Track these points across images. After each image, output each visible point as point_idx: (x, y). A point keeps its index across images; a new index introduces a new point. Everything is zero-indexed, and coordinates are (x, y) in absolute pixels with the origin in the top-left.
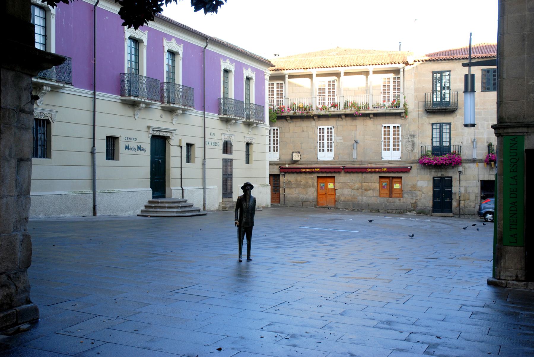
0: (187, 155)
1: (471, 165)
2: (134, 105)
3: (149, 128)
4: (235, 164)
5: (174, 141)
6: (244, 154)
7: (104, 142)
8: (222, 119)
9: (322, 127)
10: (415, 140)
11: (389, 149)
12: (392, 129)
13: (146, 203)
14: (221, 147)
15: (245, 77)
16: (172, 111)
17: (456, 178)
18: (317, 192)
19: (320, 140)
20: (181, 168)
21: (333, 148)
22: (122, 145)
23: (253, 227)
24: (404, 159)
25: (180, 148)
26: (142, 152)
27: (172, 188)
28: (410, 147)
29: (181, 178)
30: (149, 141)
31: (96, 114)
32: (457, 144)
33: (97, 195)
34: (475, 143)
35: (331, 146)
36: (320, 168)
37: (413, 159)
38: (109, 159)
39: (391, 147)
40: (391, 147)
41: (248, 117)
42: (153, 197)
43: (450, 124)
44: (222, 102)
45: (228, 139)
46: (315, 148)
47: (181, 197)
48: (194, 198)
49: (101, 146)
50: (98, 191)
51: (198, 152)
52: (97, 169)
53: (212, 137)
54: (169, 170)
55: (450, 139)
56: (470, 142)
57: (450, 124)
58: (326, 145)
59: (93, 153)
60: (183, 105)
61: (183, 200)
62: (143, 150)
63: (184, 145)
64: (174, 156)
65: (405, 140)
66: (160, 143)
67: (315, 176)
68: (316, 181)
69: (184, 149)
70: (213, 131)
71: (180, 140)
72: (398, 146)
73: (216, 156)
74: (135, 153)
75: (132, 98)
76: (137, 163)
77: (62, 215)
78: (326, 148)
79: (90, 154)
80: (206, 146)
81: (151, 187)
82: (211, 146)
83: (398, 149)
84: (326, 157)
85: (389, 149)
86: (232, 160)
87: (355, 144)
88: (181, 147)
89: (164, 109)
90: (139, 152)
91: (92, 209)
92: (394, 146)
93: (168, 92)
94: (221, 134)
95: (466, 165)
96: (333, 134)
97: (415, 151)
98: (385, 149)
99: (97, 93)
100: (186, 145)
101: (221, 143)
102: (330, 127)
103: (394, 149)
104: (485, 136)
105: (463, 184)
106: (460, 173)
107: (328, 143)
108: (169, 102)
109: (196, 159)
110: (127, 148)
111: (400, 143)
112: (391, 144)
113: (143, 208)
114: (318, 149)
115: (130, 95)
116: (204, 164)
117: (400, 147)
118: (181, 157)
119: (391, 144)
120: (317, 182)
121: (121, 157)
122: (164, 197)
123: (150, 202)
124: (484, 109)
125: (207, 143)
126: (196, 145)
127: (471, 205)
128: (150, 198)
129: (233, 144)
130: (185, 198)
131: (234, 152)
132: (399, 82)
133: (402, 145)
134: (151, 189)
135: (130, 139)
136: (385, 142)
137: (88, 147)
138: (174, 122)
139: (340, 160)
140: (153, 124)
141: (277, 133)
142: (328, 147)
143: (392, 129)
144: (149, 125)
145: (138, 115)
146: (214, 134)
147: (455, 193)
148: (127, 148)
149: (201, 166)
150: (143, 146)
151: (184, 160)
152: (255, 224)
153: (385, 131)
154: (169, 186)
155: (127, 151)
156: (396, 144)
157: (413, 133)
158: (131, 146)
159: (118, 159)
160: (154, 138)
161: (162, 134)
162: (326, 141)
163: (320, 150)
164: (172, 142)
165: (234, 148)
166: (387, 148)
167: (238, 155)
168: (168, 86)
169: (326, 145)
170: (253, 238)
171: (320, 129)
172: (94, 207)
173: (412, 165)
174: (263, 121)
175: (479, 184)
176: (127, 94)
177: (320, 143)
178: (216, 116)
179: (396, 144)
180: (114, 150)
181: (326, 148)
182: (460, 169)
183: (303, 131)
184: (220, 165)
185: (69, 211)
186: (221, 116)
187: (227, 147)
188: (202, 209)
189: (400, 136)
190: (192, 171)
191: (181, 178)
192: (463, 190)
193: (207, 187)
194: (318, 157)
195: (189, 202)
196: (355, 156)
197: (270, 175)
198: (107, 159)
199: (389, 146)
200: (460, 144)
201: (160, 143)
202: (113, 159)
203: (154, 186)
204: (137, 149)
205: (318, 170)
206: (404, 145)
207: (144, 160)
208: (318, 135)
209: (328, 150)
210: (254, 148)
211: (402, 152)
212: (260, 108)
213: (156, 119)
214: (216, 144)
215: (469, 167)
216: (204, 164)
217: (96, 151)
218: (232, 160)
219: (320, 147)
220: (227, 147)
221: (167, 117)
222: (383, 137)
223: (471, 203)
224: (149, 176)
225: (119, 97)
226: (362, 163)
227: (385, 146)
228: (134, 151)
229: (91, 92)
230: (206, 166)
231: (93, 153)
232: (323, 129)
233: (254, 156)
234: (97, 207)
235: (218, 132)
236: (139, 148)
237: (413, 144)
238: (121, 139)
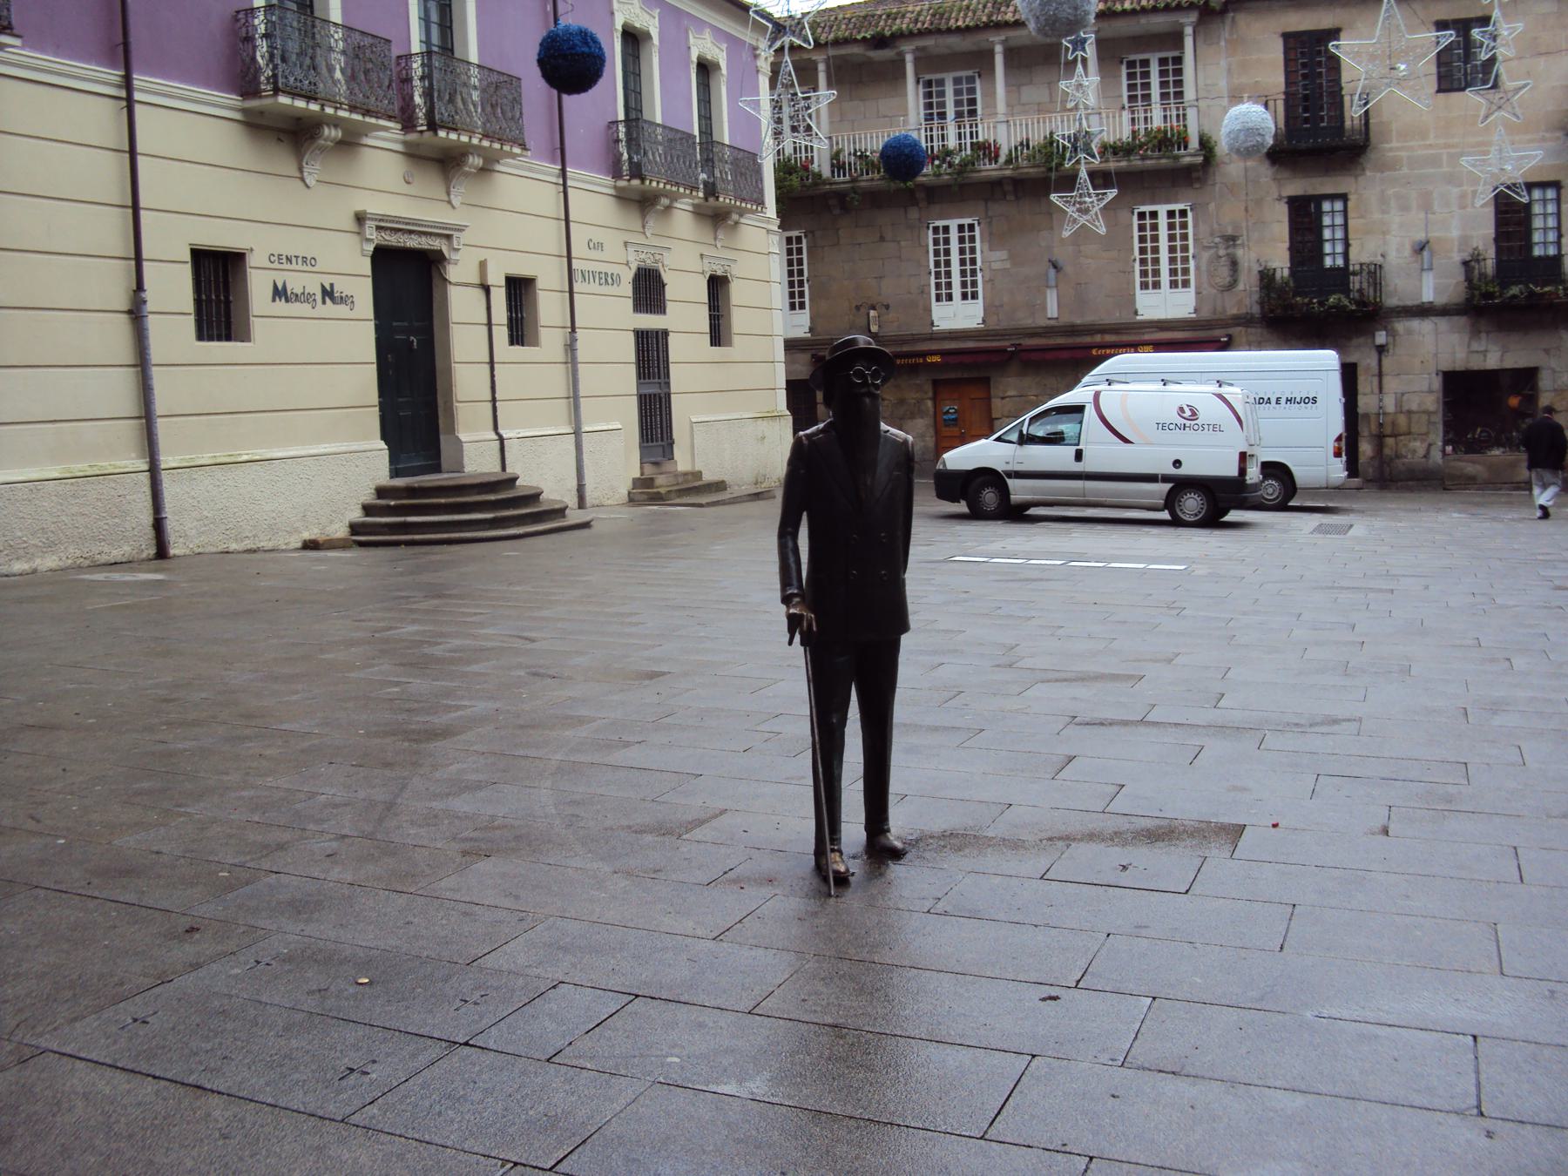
0: (510, 319)
1: (1415, 324)
2: (297, 135)
3: (360, 218)
4: (677, 348)
5: (459, 270)
6: (704, 312)
7: (186, 273)
8: (622, 197)
9: (940, 223)
10: (1240, 252)
11: (1157, 285)
12: (1163, 221)
13: (368, 496)
14: (627, 289)
15: (695, 59)
16: (447, 163)
17: (1368, 368)
18: (937, 432)
19: (937, 264)
20: (492, 363)
21: (980, 289)
22: (258, 285)
23: (905, 640)
24: (1206, 314)
25: (480, 294)
26: (342, 310)
27: (463, 437)
28: (1224, 273)
29: (494, 400)
30: (366, 266)
31: (142, 162)
32: (1365, 259)
33: (166, 480)
34: (1425, 253)
35: (974, 284)
36: (942, 353)
37: (1235, 311)
38: (211, 339)
39: (1165, 277)
40: (1165, 277)
41: (711, 191)
42: (395, 473)
43: (1344, 197)
44: (622, 136)
45: (649, 263)
46: (924, 291)
47: (498, 469)
48: (544, 472)
49: (172, 289)
50: (166, 460)
51: (548, 307)
52: (158, 376)
53: (594, 254)
54: (448, 371)
55: (1347, 245)
56: (1407, 252)
57: (1344, 197)
58: (956, 279)
59: (136, 313)
60: (486, 136)
61: (504, 477)
62: (343, 300)
63: (497, 279)
64: (467, 319)
65: (1206, 255)
66: (407, 281)
67: (924, 381)
68: (930, 394)
69: (499, 297)
70: (598, 235)
71: (483, 265)
72: (1186, 271)
73: (611, 322)
74: (314, 313)
75: (284, 100)
76: (323, 351)
77: (18, 567)
78: (957, 290)
79: (124, 318)
80: (577, 287)
81: (384, 437)
82: (594, 287)
83: (1186, 284)
84: (958, 315)
85: (1157, 285)
86: (666, 333)
87: (1052, 272)
88: (486, 289)
89: (413, 154)
90: (330, 309)
91: (150, 533)
92: (1173, 272)
93: (428, 94)
94: (626, 244)
95: (1401, 326)
96: (978, 244)
97: (1241, 287)
98: (1144, 286)
99: (139, 80)
100: (503, 283)
101: (628, 276)
102: (966, 221)
103: (1174, 284)
104: (1455, 233)
105: (1391, 384)
106: (1381, 350)
107: (963, 273)
108: (433, 126)
109: (543, 331)
110: (279, 293)
111: (1192, 264)
112: (1164, 267)
113: (356, 515)
114: (933, 292)
115: (277, 91)
116: (571, 347)
117: (1192, 277)
118: (489, 324)
119: (1164, 267)
120: (934, 399)
121: (257, 326)
122: (437, 469)
123: (381, 492)
124: (1447, 146)
125: (578, 276)
126: (540, 284)
127: (1414, 451)
128: (382, 476)
129: (666, 277)
130: (511, 470)
131: (670, 306)
132: (1179, 72)
133: (1197, 268)
134: (383, 445)
135: (289, 260)
136: (1143, 262)
137: (113, 288)
138: (456, 201)
139: (1004, 325)
140: (376, 206)
141: (800, 251)
142: (964, 284)
143: (1163, 221)
144: (359, 208)
145: (314, 170)
146: (599, 246)
147: (1366, 416)
148: (279, 293)
149: (559, 355)
150: (341, 287)
151: (501, 334)
152: (913, 620)
153: (1142, 228)
154: (452, 430)
155: (281, 307)
156: (1179, 266)
157: (1230, 231)
158: (295, 284)
159: (245, 336)
160: (384, 259)
161: (413, 242)
162: (955, 268)
163: (938, 298)
164: (453, 273)
165: (670, 293)
166: (1150, 279)
167: (684, 315)
168: (427, 65)
169: (956, 279)
170: (903, 710)
171: (936, 230)
172: (158, 525)
173: (1231, 331)
174: (760, 202)
175: (1437, 383)
176: (266, 87)
177: (938, 275)
178: (604, 182)
179: (1179, 266)
180: (228, 303)
181: (957, 290)
182: (1381, 337)
183: (882, 239)
184: (627, 349)
185: (50, 546)
186: (622, 183)
187: (649, 289)
188: (571, 500)
189: (1191, 242)
190: (530, 373)
191: (494, 400)
192: (1390, 404)
193: (586, 428)
194: (935, 317)
195: (527, 480)
196: (1052, 310)
197: (788, 382)
198: (200, 337)
199: (1156, 273)
200: (1379, 260)
201: (407, 281)
202: (228, 338)
203: (391, 430)
204: (319, 297)
205: (937, 359)
206: (1204, 268)
207: (354, 337)
208: (931, 248)
209: (964, 296)
210: (738, 293)
211: (1198, 293)
212: (747, 163)
213: (382, 182)
214: (609, 279)
215: (1409, 332)
216: (571, 347)
217: (150, 307)
218: (666, 333)
219: (938, 286)
220: (649, 289)
221: (430, 183)
222: (1136, 245)
223: (1418, 444)
224: (373, 396)
225: (233, 99)
226: (1072, 330)
227: (1144, 274)
228: (307, 306)
229: (115, 75)
230: (581, 356)
231: (136, 313)
232: (946, 229)
233: (739, 320)
234: (171, 525)
235: (607, 236)
236: (328, 293)
237: (1234, 264)
238: (252, 261)
